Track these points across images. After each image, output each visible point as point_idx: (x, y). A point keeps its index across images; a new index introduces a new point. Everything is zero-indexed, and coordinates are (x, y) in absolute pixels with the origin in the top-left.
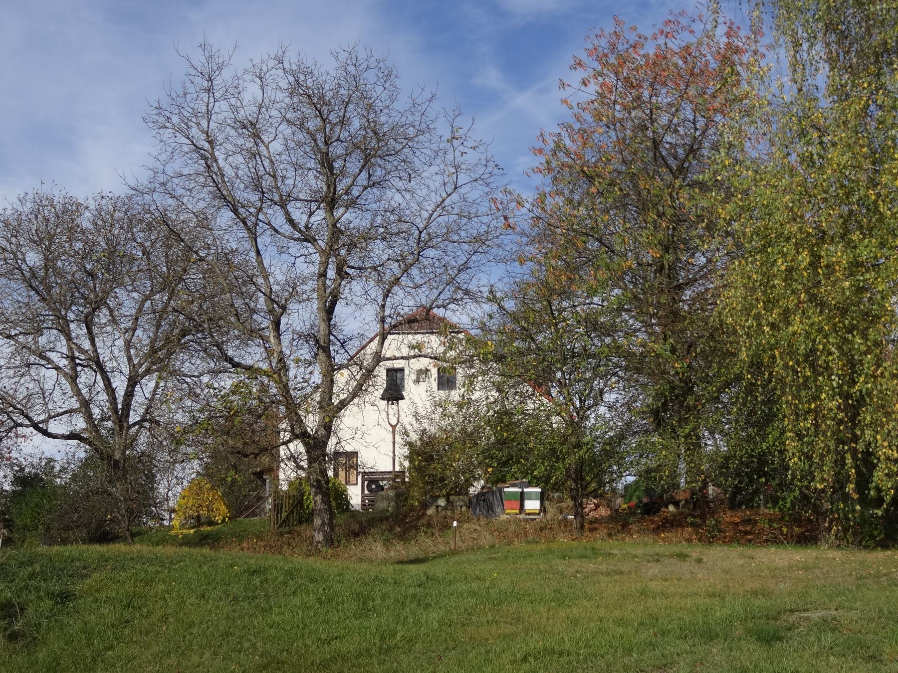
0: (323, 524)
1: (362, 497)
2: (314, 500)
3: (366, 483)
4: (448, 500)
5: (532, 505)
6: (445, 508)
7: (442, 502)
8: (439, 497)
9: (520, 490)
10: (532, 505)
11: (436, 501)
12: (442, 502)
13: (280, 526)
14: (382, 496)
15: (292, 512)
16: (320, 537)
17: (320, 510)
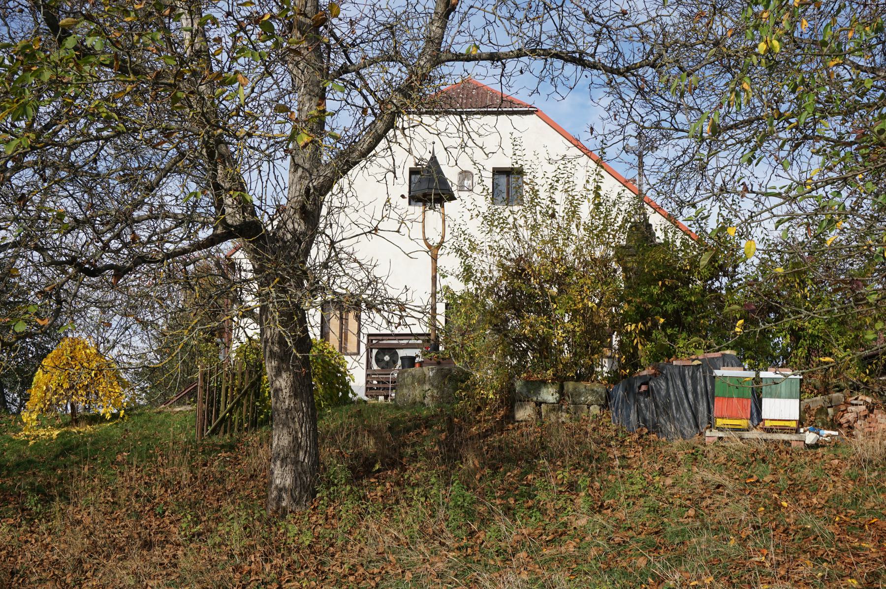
0: (296, 446)
1: (368, 375)
2: (280, 384)
3: (375, 352)
4: (561, 391)
5: (781, 409)
6: (557, 407)
7: (549, 395)
8: (544, 383)
9: (752, 374)
10: (781, 409)
11: (537, 391)
12: (549, 395)
13: (214, 432)
14: (413, 376)
15: (239, 403)
16: (282, 477)
17: (287, 411)
